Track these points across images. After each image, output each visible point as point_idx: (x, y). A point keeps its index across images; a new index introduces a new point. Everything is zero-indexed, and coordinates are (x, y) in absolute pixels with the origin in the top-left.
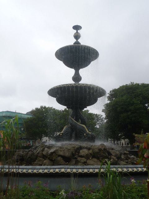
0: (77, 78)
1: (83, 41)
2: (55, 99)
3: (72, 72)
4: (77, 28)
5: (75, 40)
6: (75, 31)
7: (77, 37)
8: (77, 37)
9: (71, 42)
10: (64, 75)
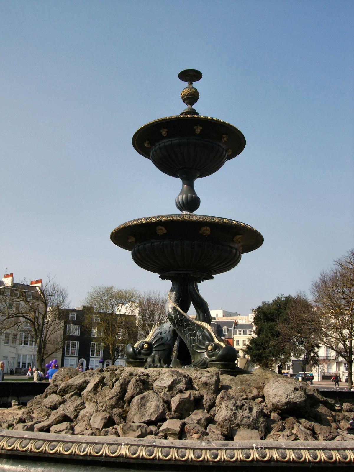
0: (191, 203)
1: (204, 109)
2: (129, 253)
4: (191, 76)
5: (185, 107)
6: (186, 84)
7: (191, 98)
8: (191, 98)
9: (176, 109)
10: (157, 195)
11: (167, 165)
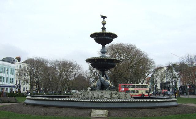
1: (107, 31)
3: (100, 46)
4: (104, 17)
9: (100, 31)
11: (98, 41)
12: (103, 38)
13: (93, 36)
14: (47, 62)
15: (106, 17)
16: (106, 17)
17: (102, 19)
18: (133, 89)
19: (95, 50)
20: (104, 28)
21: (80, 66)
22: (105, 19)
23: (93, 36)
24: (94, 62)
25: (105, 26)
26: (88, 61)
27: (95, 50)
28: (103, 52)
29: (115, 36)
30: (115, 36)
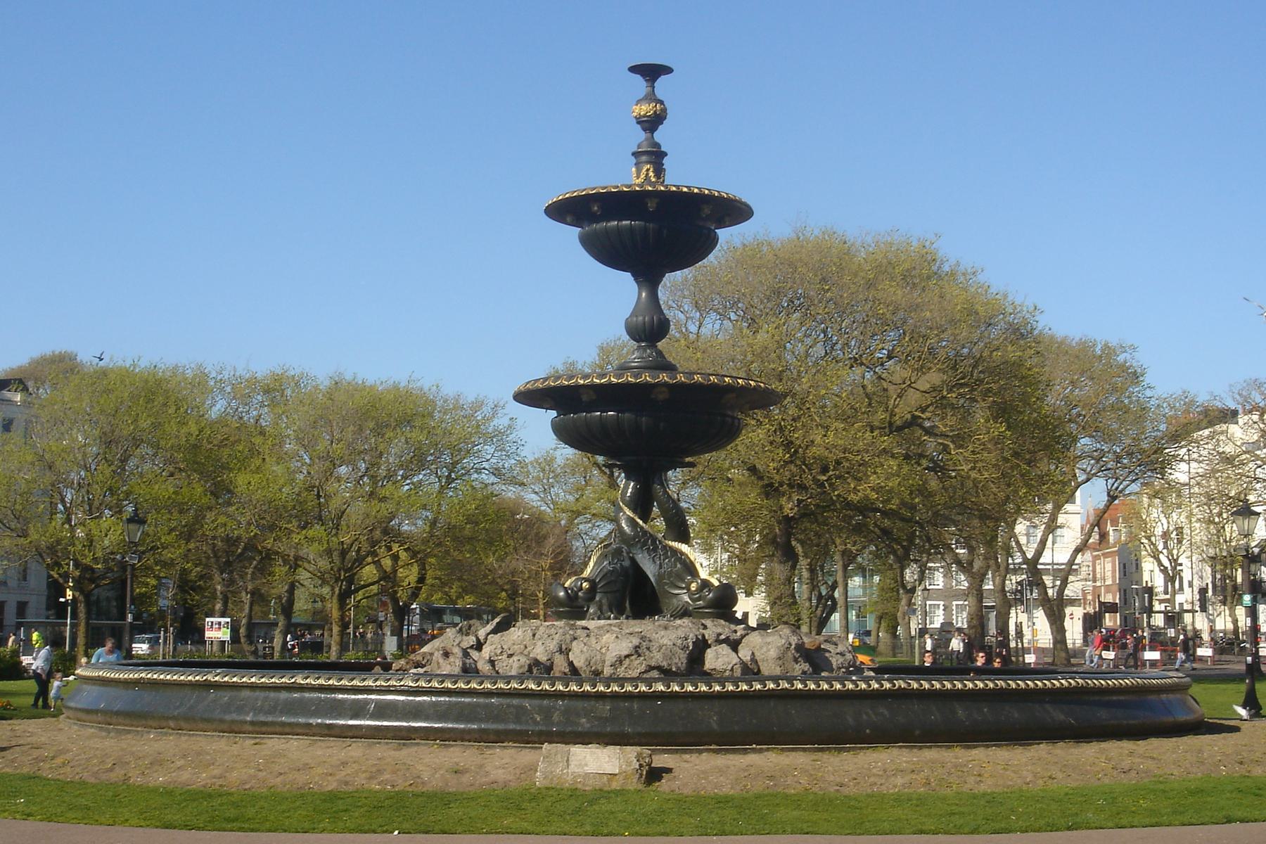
3: (619, 292)
4: (651, 72)
9: (627, 175)
11: (609, 252)
12: (651, 230)
13: (568, 210)
14: (200, 382)
15: (667, 70)
16: (667, 70)
17: (639, 82)
18: (961, 809)
19: (586, 317)
20: (656, 156)
21: (486, 410)
22: (662, 82)
23: (568, 210)
24: (569, 403)
25: (659, 136)
26: (531, 397)
27: (586, 317)
28: (651, 330)
29: (733, 211)
30: (733, 211)
